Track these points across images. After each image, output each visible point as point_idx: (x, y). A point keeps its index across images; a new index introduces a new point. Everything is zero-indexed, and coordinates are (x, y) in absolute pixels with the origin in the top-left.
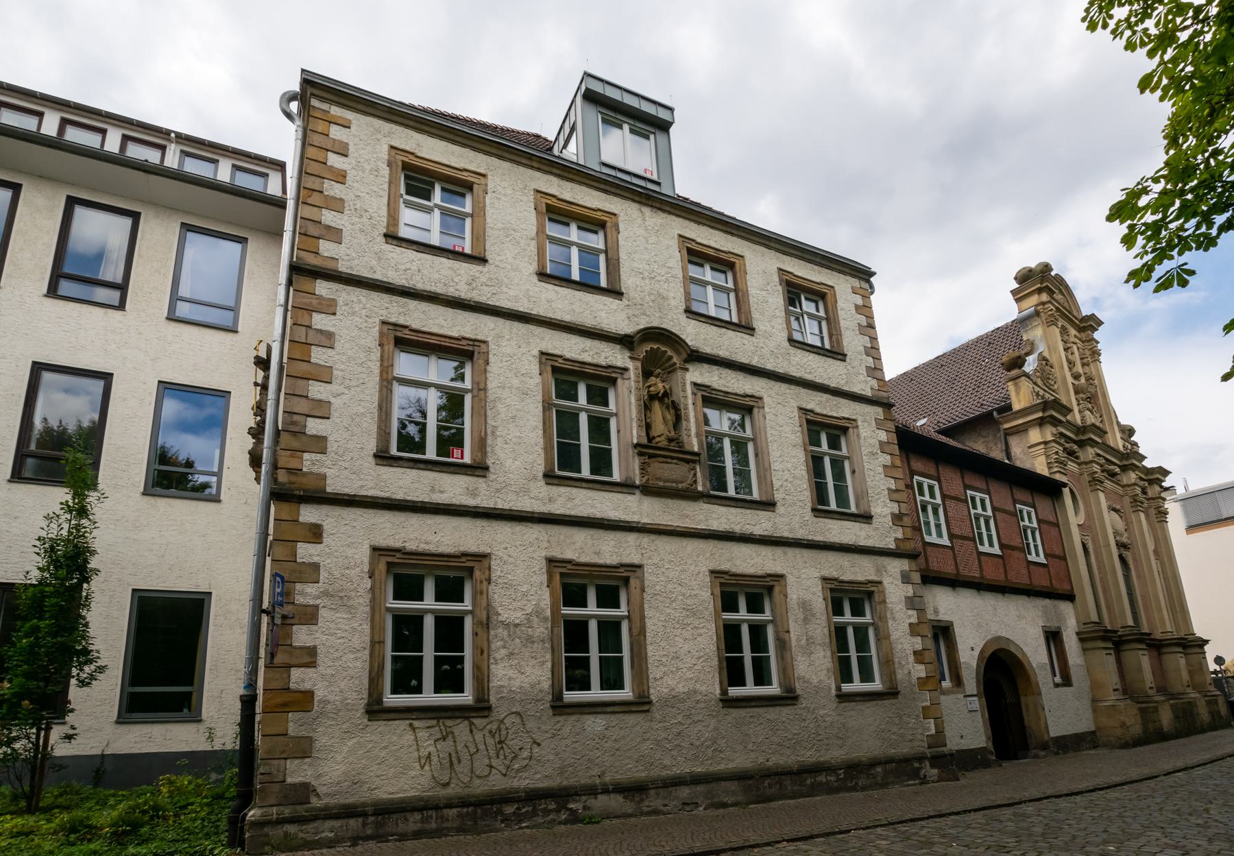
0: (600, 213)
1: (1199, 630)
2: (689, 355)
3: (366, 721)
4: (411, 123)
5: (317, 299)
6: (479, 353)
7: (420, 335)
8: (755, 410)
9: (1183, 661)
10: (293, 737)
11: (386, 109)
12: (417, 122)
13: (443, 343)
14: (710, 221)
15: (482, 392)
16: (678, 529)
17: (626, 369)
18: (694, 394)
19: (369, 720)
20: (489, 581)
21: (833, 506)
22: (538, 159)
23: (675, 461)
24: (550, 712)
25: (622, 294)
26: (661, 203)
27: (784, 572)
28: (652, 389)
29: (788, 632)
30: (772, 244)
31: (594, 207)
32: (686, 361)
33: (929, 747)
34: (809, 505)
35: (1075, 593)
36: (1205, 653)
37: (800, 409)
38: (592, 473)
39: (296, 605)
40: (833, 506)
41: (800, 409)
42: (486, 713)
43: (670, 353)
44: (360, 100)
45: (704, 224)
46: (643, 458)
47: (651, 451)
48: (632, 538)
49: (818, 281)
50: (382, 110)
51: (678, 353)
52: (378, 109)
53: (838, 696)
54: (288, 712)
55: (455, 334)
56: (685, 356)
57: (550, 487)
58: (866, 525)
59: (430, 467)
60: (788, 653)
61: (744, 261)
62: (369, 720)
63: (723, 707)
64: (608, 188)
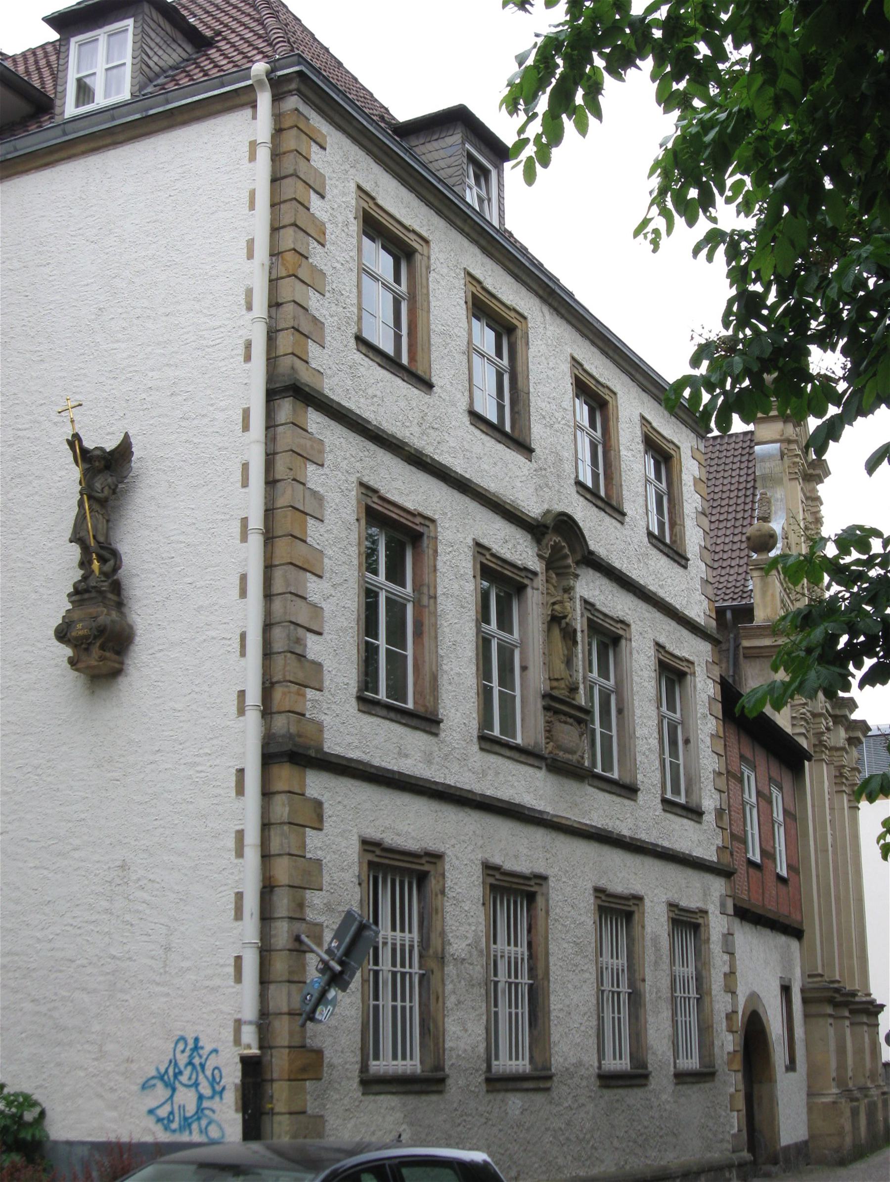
0: (513, 314)
1: (878, 994)
2: (584, 557)
3: (360, 1094)
4: (375, 150)
5: (310, 439)
6: (428, 537)
7: (386, 505)
8: (623, 642)
9: (831, 1031)
10: (310, 1116)
11: (359, 127)
12: (380, 148)
13: (402, 520)
14: (595, 334)
15: (432, 601)
16: (555, 819)
17: (535, 574)
18: (582, 616)
19: (363, 1094)
20: (443, 893)
21: (382, 695)
22: (472, 223)
23: (569, 720)
24: (484, 1087)
25: (624, 514)
26: (559, 303)
27: (549, 872)
28: (557, 607)
29: (644, 980)
30: (638, 376)
31: (508, 303)
32: (578, 563)
33: (734, 1152)
34: (353, 690)
35: (805, 928)
36: (878, 1025)
37: (362, 484)
38: (501, 733)
39: (308, 923)
40: (382, 695)
41: (362, 484)
42: (643, 1082)
43: (567, 551)
44: (416, 174)
45: (587, 338)
46: (548, 714)
47: (557, 706)
48: (539, 835)
49: (669, 437)
50: (355, 127)
51: (573, 550)
52: (351, 123)
53: (488, 1080)
54: (305, 1080)
55: (410, 506)
56: (579, 557)
57: (485, 755)
58: (627, 802)
59: (392, 715)
60: (643, 1011)
61: (616, 398)
62: (363, 1094)
63: (488, 1091)
64: (520, 274)
